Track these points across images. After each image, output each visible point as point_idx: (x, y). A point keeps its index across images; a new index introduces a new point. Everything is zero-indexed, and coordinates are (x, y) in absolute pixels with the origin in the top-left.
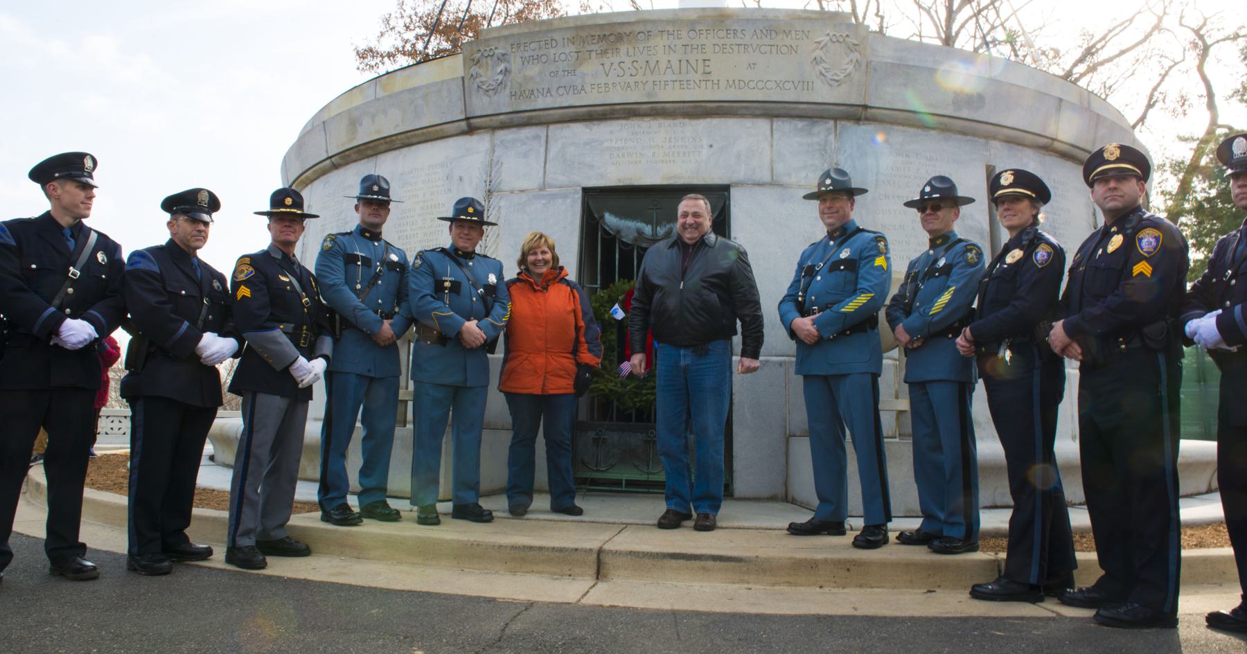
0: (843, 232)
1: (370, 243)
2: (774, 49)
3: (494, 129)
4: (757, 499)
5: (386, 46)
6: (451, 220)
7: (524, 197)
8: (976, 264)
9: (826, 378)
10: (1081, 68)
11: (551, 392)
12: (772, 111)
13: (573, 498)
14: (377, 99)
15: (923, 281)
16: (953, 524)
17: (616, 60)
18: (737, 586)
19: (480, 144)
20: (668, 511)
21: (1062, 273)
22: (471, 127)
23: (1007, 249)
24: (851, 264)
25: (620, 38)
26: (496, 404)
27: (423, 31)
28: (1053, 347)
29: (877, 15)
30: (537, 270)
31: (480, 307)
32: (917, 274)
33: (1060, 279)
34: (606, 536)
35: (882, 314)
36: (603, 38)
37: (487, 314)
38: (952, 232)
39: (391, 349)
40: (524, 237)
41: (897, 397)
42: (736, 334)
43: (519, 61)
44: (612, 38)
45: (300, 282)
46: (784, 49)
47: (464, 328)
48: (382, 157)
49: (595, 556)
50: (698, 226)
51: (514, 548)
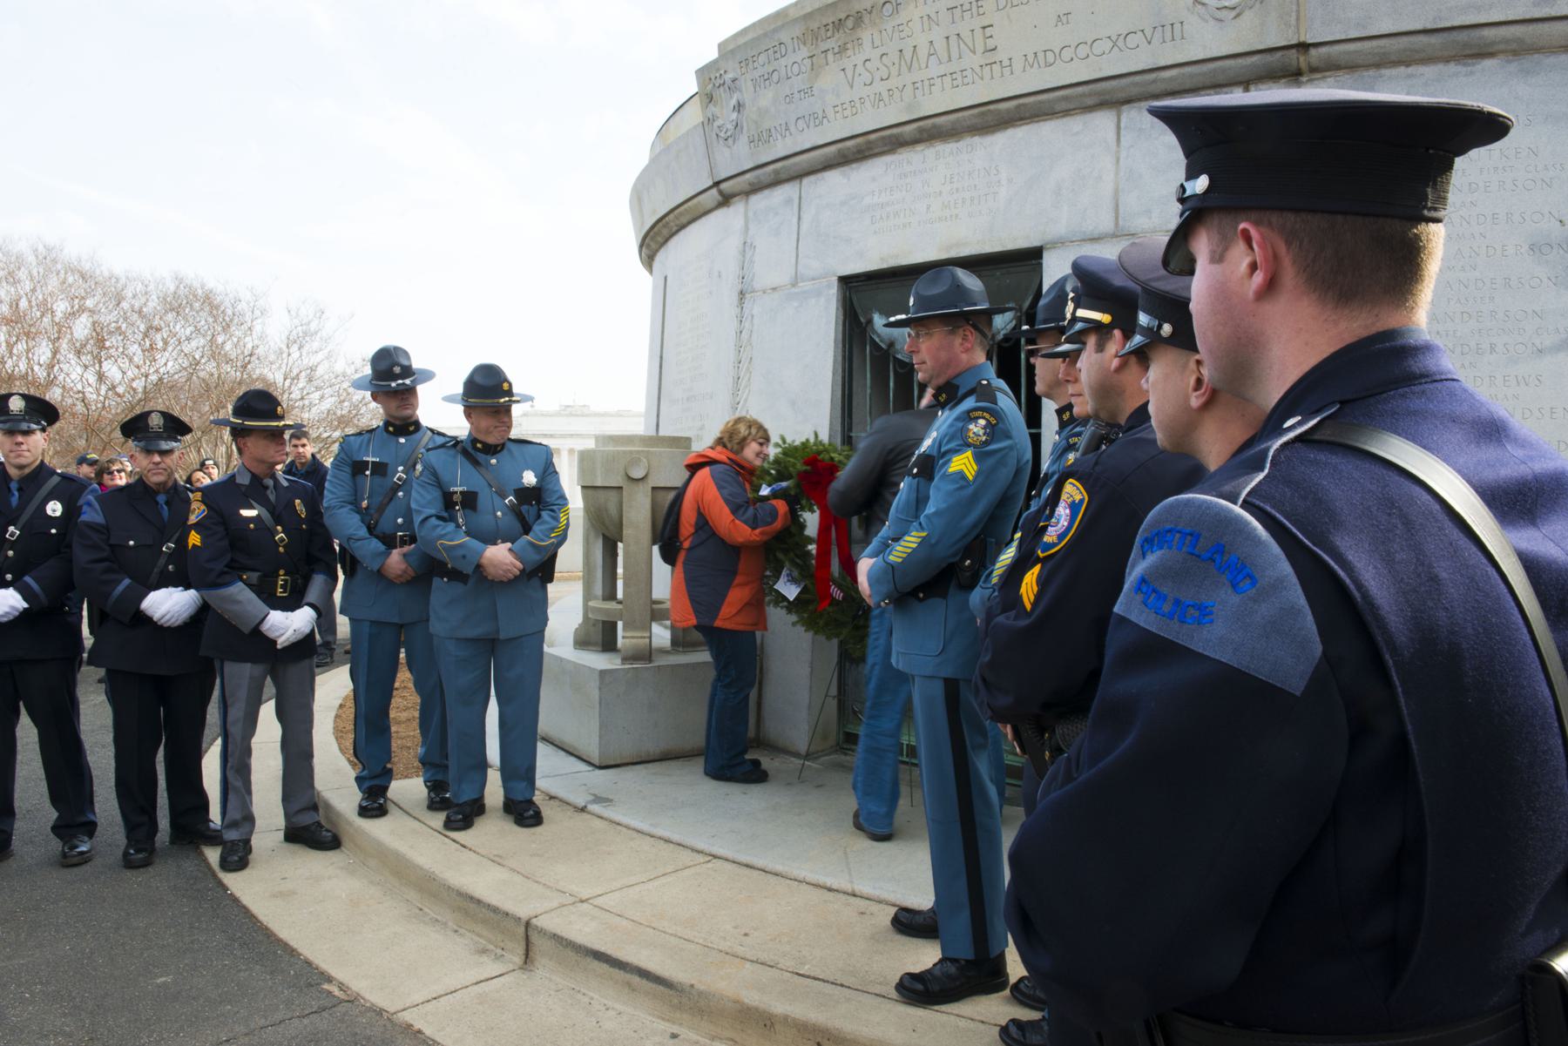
19: (733, 216)
36: (839, 25)
37: (527, 529)
43: (750, 83)
44: (850, 23)
45: (272, 513)
47: (484, 561)
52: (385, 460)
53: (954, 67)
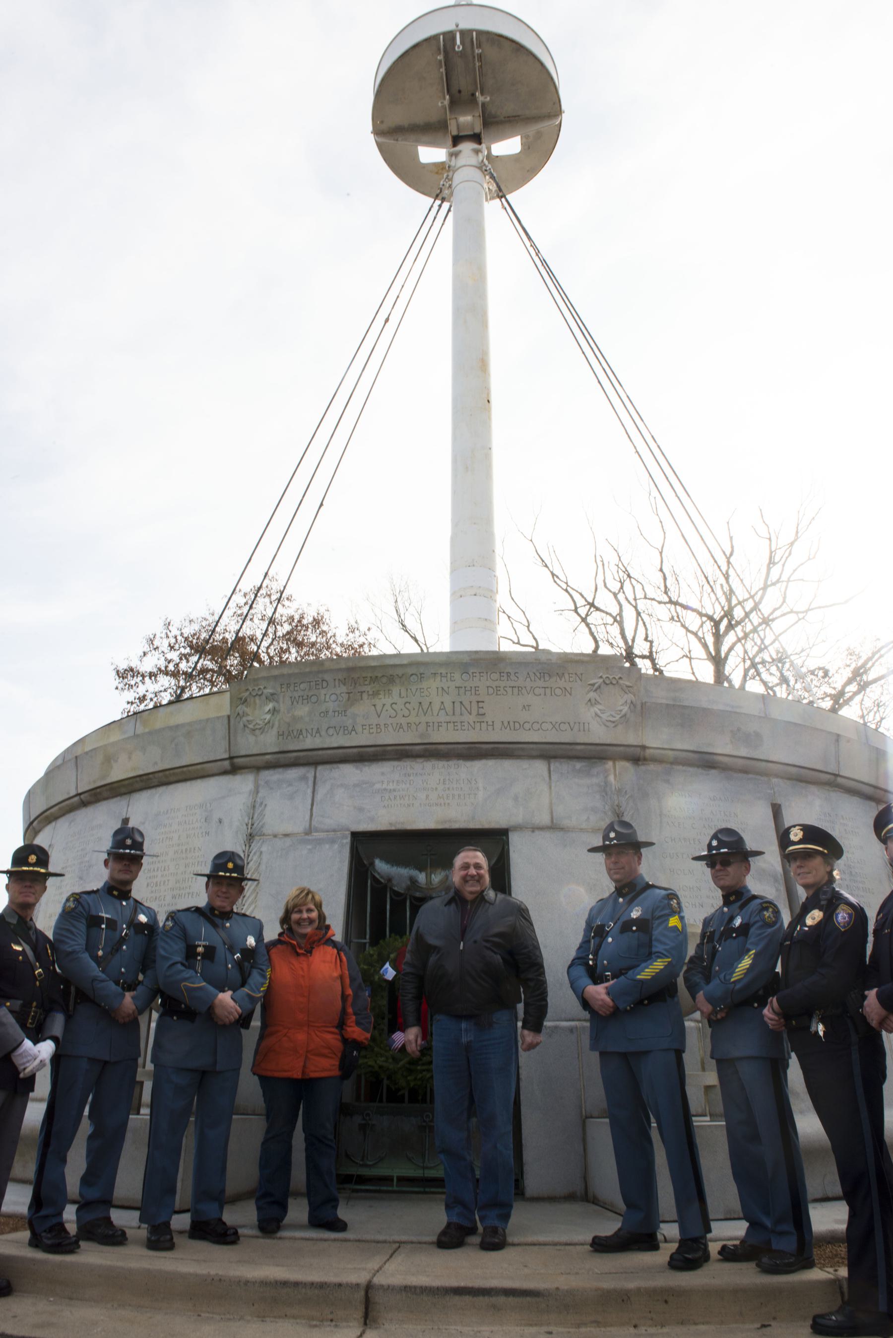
0: (629, 888)
1: (117, 902)
2: (548, 691)
3: (258, 769)
4: (551, 1199)
5: (147, 666)
6: (209, 876)
7: (288, 841)
8: (775, 923)
9: (624, 1056)
10: (853, 688)
11: (313, 1075)
12: (551, 753)
13: (335, 1208)
14: (136, 736)
15: (719, 941)
16: (782, 1234)
17: (388, 701)
18: (533, 1330)
19: (243, 783)
20: (449, 1225)
21: (866, 935)
22: (234, 766)
23: (806, 909)
24: (643, 924)
25: (391, 680)
26: (249, 1087)
27: (188, 650)
28: (869, 1020)
29: (646, 639)
30: (301, 929)
31: (236, 976)
32: (713, 933)
33: (866, 942)
34: (374, 1264)
35: (680, 980)
37: (243, 984)
38: (745, 887)
39: (132, 1026)
40: (289, 892)
41: (703, 1069)
42: (520, 1002)
44: (384, 680)
45: (34, 950)
46: (558, 691)
47: (217, 1001)
48: (136, 796)
49: (362, 1293)
50: (479, 878)
51: (265, 1283)
52: (115, 918)
53: (454, 719)
